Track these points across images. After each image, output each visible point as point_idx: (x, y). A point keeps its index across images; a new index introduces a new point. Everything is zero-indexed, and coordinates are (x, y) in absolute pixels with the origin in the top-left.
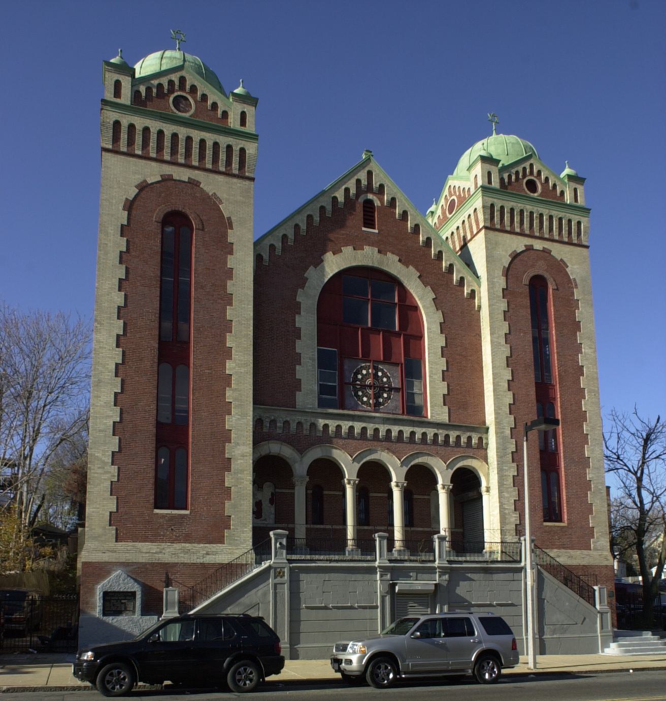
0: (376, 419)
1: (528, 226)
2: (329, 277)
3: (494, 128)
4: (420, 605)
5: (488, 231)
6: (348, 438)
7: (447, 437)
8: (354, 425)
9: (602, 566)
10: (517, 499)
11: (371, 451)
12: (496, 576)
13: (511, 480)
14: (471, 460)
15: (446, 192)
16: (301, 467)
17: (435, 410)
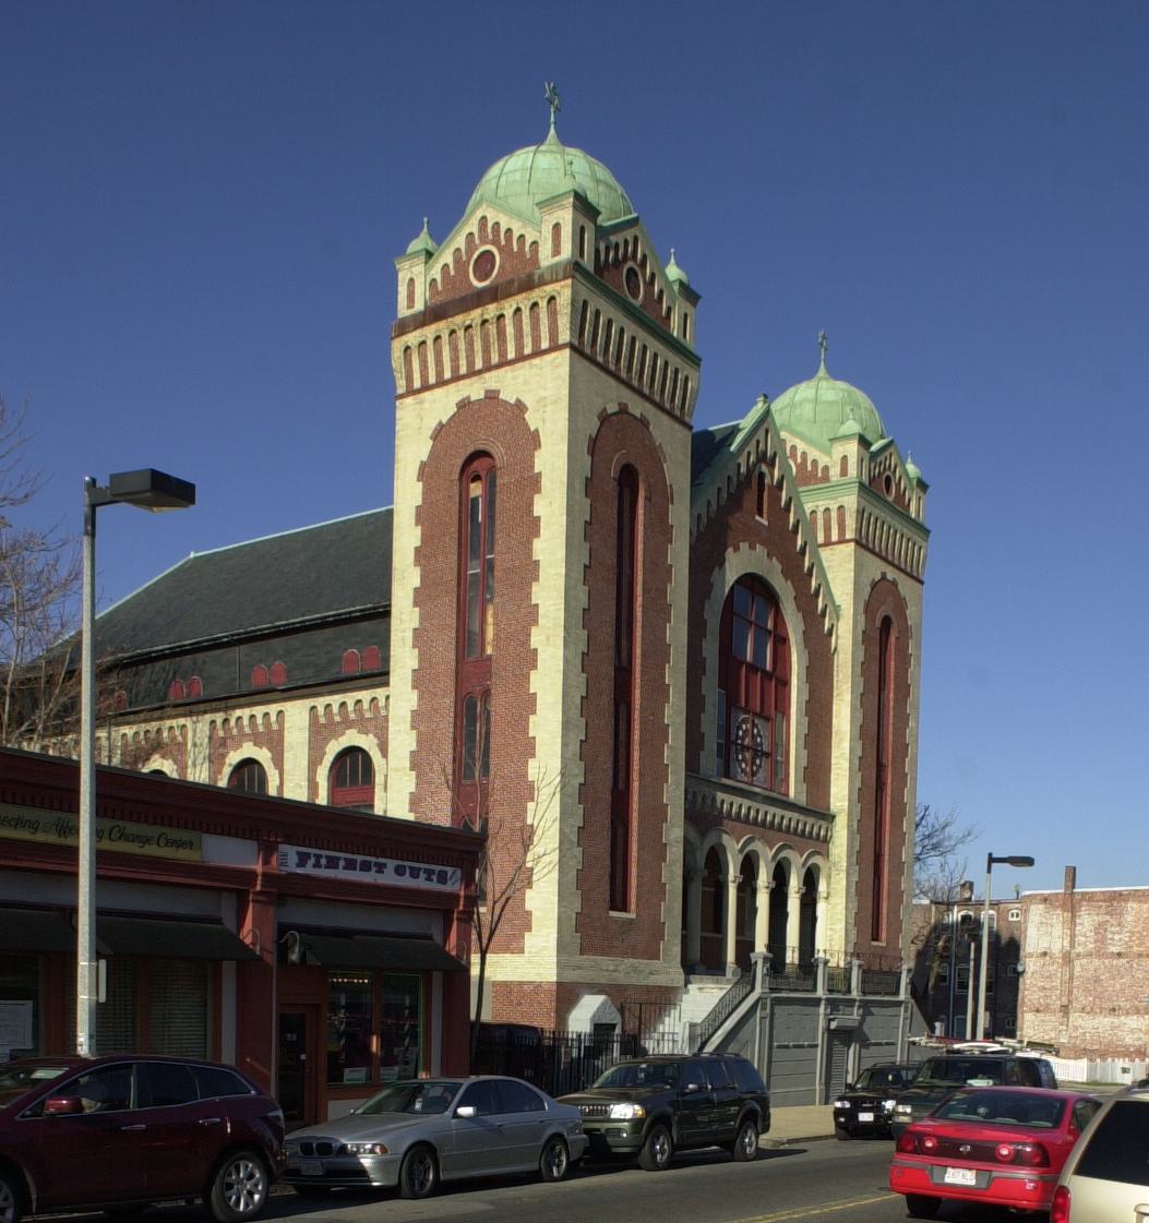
0: (759, 797)
1: (590, 340)
2: (731, 584)
3: (552, 119)
5: (858, 547)
6: (746, 823)
15: (472, 226)
17: (794, 790)
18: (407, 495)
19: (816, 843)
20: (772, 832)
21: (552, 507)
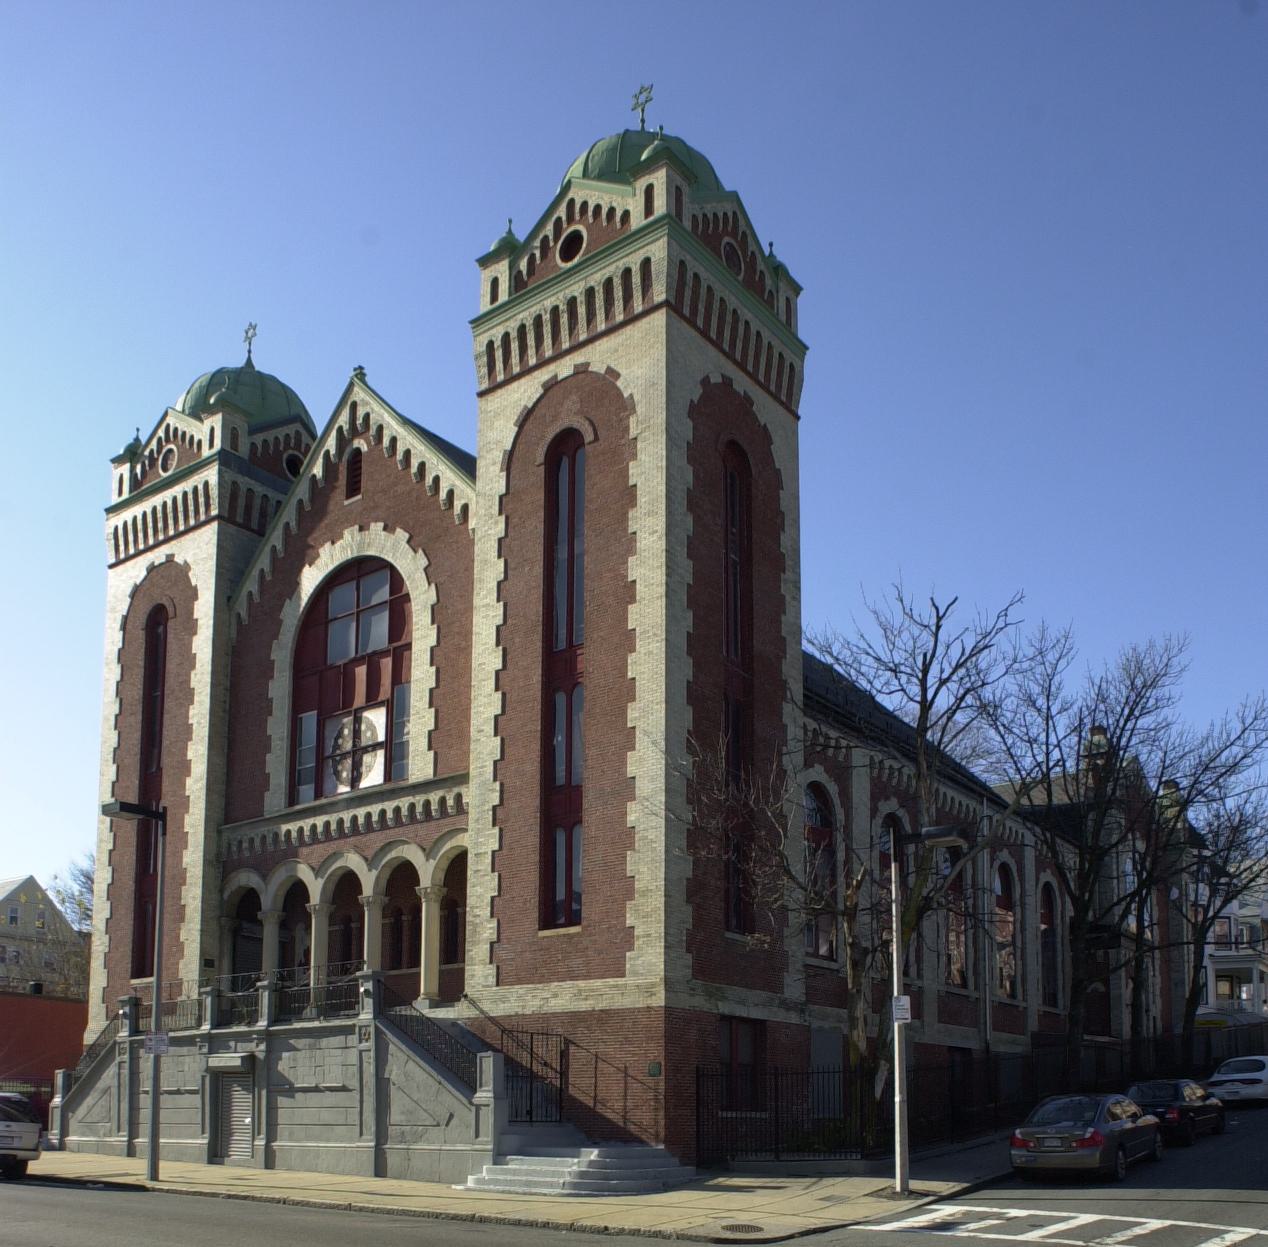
4: (243, 1090)
6: (340, 838)
7: (427, 804)
8: (385, 807)
9: (639, 1010)
10: (496, 894)
11: (336, 855)
12: (324, 1042)
13: (488, 860)
14: (461, 835)
16: (270, 898)
18: (285, 465)
19: (412, 828)
20: (372, 836)
21: (649, 470)
